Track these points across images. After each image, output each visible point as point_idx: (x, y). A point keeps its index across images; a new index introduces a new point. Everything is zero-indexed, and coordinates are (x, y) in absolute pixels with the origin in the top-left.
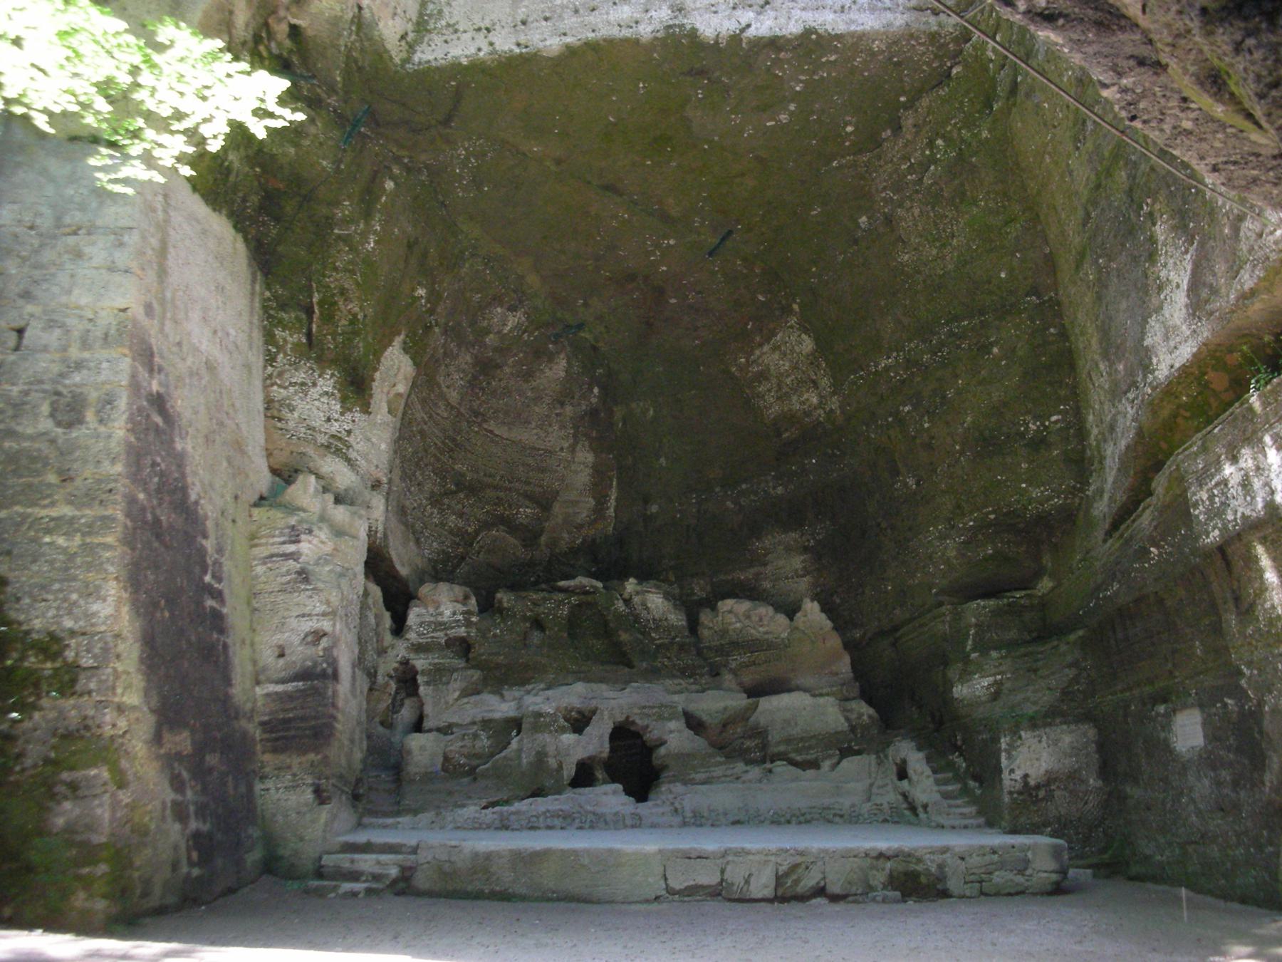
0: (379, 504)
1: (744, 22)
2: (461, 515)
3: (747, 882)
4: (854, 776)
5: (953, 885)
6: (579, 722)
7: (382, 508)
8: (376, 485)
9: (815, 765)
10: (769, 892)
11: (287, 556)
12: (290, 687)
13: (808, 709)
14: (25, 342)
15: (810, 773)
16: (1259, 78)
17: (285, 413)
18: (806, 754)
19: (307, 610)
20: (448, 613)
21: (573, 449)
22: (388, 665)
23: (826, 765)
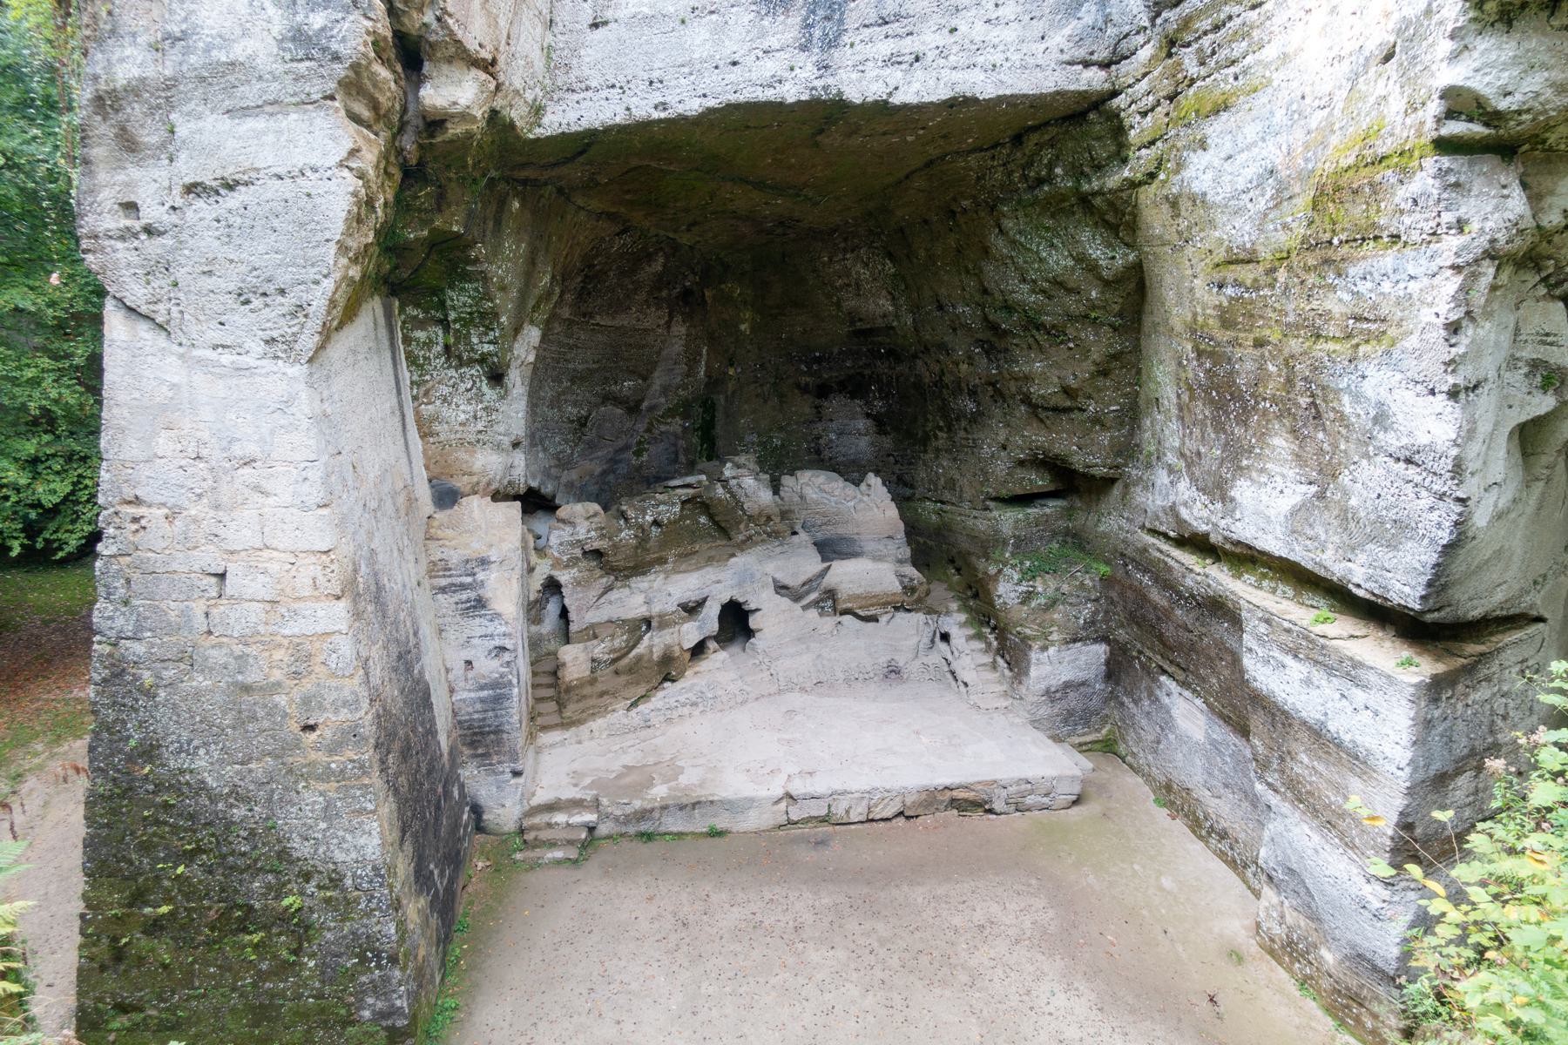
1: (892, 83)
2: (575, 404)
3: (847, 812)
4: (910, 628)
5: (998, 805)
6: (692, 609)
7: (523, 464)
9: (873, 619)
10: (863, 818)
11: (463, 587)
12: (485, 693)
13: (874, 571)
14: (229, 591)
15: (871, 625)
16: (1493, 241)
17: (437, 427)
18: (866, 612)
19: (489, 631)
20: (583, 531)
21: (668, 325)
23: (883, 619)
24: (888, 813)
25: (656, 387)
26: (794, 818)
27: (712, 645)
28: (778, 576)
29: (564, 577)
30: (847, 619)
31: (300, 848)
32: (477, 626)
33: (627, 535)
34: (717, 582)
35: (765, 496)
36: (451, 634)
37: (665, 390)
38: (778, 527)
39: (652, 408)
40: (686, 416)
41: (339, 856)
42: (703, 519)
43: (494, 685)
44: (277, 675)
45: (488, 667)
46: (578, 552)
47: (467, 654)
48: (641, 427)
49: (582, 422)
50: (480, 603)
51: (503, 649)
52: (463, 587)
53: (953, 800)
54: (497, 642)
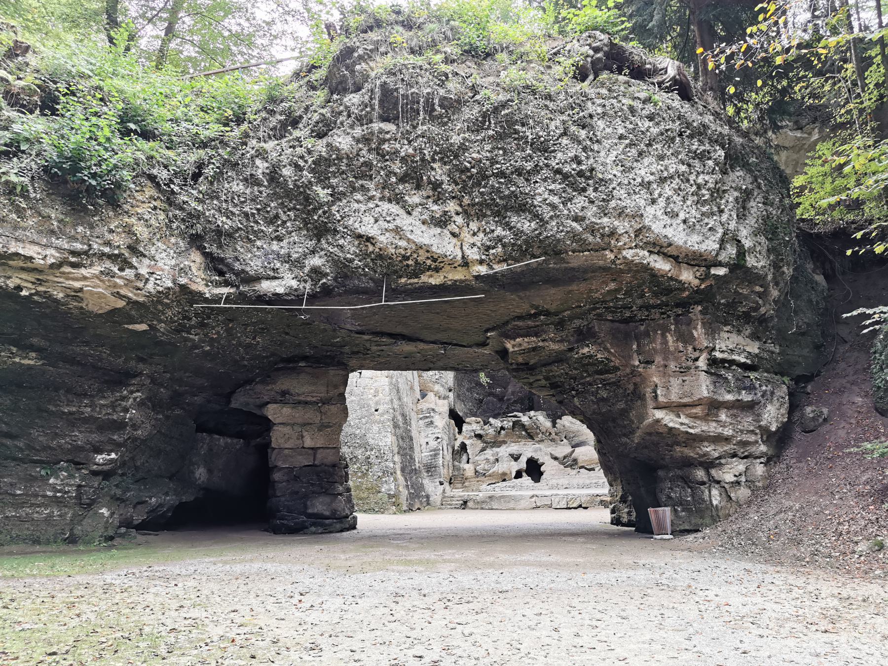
0: (451, 394)
6: (516, 458)
8: (450, 391)
11: (427, 417)
22: (457, 444)
24: (575, 505)
25: (510, 391)
26: (539, 505)
27: (524, 474)
28: (553, 453)
29: (467, 442)
30: (583, 470)
31: (371, 442)
32: (430, 430)
33: (491, 431)
34: (528, 450)
35: (548, 424)
36: (422, 434)
37: (513, 393)
38: (552, 438)
39: (508, 400)
40: (522, 404)
41: (380, 444)
42: (523, 433)
43: (434, 450)
44: (370, 396)
45: (433, 444)
46: (473, 434)
47: (427, 440)
48: (504, 407)
49: (481, 401)
50: (432, 422)
51: (438, 438)
52: (427, 417)
53: (602, 501)
54: (436, 435)
